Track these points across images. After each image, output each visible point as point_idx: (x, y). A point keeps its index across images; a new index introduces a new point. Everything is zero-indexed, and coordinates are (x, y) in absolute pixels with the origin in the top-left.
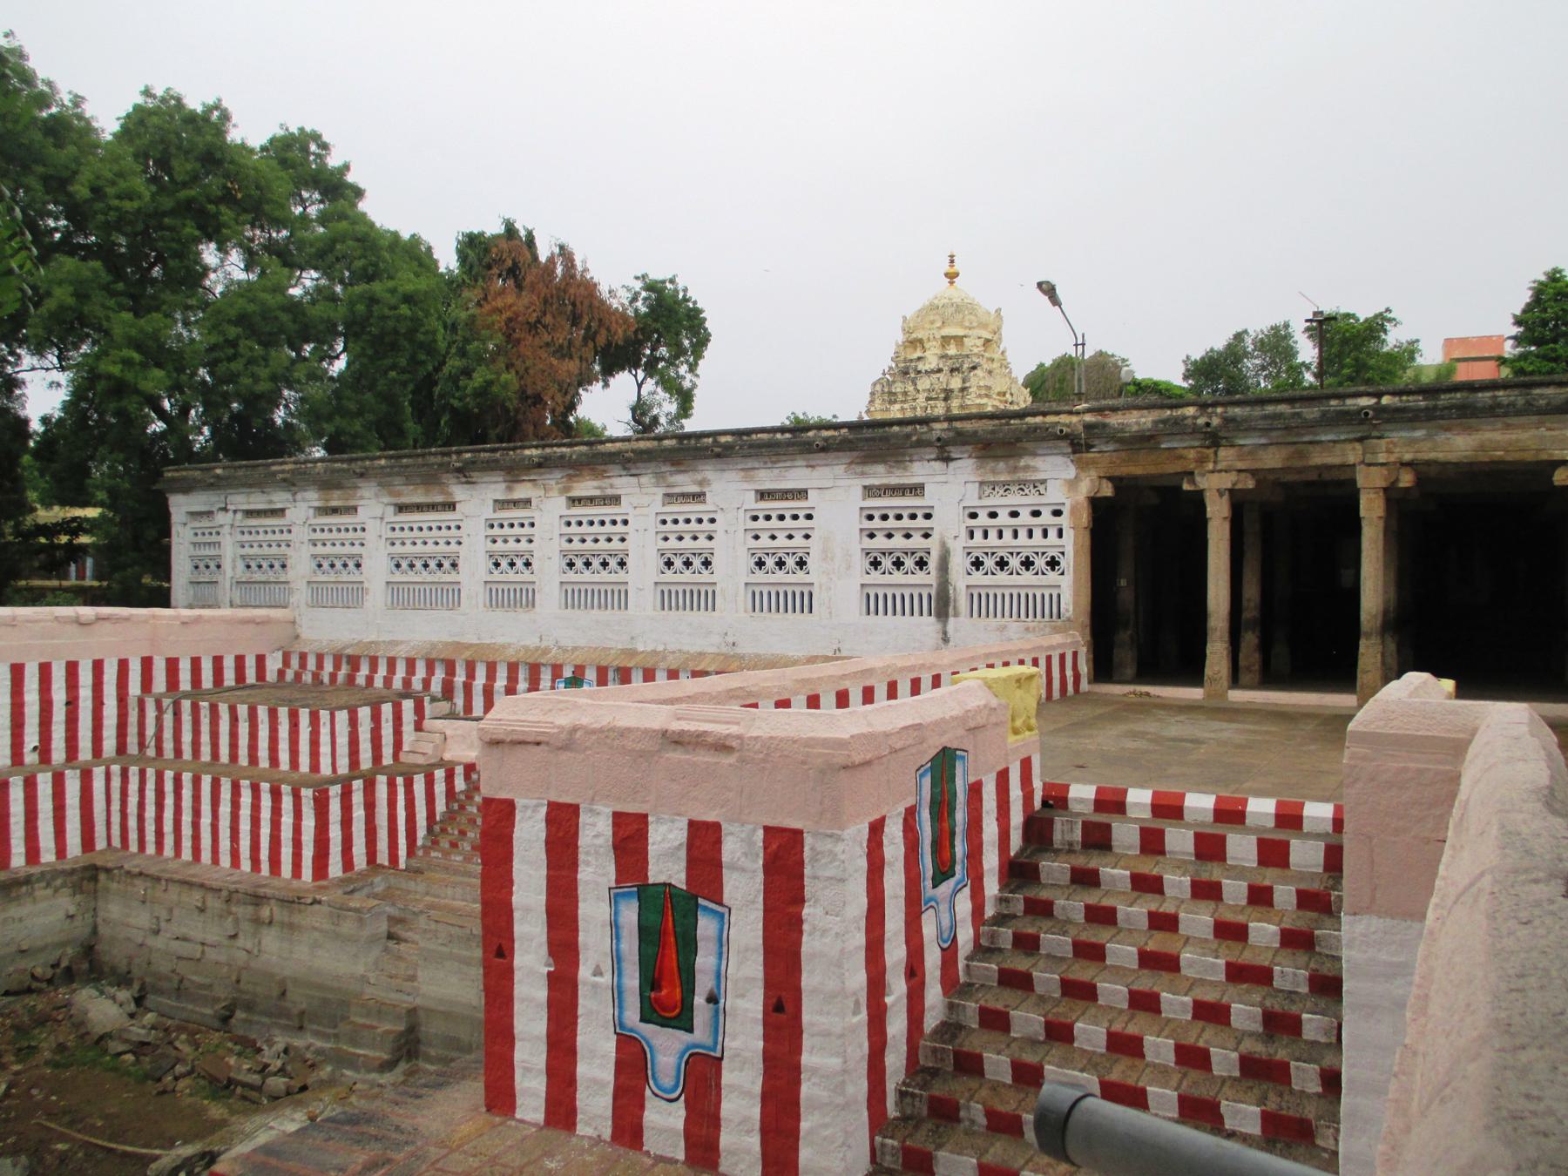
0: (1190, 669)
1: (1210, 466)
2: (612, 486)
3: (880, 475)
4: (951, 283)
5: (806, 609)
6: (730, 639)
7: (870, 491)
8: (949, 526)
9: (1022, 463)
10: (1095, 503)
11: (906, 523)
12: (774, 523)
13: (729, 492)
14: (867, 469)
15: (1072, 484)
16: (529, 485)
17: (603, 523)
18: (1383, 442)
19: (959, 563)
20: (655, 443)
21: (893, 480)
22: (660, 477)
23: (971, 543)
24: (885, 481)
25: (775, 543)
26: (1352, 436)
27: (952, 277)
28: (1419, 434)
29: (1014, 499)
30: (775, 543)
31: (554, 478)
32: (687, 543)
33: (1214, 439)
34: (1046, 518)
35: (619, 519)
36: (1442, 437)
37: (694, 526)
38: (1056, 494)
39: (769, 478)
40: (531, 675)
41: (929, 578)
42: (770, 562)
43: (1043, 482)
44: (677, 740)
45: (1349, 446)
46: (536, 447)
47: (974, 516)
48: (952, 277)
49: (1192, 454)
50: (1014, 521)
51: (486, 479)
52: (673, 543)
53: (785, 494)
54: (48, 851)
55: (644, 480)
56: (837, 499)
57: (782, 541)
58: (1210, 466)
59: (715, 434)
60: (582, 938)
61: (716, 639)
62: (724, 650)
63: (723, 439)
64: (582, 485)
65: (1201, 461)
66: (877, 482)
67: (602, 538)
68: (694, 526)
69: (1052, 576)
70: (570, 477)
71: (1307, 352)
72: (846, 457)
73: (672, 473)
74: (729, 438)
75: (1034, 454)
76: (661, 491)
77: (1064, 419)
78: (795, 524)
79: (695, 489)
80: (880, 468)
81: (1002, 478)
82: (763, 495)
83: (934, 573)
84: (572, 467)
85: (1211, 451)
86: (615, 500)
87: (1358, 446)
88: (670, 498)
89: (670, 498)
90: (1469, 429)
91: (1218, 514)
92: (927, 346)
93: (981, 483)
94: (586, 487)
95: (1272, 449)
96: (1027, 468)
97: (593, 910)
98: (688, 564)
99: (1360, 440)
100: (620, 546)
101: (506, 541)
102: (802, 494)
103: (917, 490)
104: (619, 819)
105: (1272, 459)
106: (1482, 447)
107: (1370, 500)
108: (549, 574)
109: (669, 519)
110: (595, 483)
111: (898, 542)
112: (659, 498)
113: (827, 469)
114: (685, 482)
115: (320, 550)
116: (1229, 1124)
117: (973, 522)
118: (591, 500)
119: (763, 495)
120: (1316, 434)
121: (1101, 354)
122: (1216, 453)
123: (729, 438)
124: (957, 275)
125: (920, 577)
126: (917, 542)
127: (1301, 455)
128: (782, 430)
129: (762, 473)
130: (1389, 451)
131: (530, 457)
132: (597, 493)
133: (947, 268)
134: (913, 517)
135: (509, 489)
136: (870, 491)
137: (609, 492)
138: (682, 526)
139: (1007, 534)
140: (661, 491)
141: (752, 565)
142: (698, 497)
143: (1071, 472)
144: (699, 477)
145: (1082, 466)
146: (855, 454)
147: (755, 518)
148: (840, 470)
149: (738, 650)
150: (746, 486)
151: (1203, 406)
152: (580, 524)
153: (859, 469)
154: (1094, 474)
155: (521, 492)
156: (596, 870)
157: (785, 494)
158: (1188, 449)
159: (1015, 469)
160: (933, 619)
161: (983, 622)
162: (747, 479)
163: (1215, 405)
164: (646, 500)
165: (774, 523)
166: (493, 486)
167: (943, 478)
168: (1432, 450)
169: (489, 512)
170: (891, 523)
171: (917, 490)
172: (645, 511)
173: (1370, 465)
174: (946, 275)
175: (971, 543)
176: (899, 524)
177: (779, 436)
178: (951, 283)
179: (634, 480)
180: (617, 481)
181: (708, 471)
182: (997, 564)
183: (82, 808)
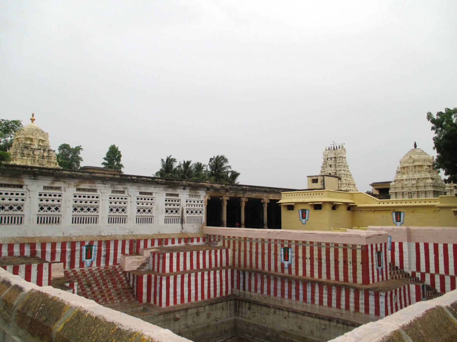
2: (95, 186)
3: (170, 191)
4: (32, 122)
5: (51, 222)
6: (132, 231)
7: (167, 195)
8: (183, 203)
9: (197, 191)
10: (208, 200)
11: (174, 202)
12: (143, 200)
13: (133, 192)
14: (168, 189)
15: (205, 197)
16: (62, 183)
17: (145, 199)
19: (185, 211)
20: (113, 176)
21: (173, 193)
22: (112, 186)
24: (171, 193)
25: (143, 206)
27: (33, 120)
29: (194, 199)
30: (87, 204)
31: (73, 182)
32: (118, 204)
33: (227, 191)
34: (200, 203)
36: (252, 194)
37: (120, 200)
38: (202, 198)
39: (144, 189)
40: (72, 245)
41: (180, 215)
42: (142, 210)
44: (379, 235)
46: (68, 171)
48: (33, 120)
49: (223, 193)
51: (44, 179)
52: (113, 204)
55: (107, 186)
56: (160, 196)
57: (89, 203)
61: (127, 231)
62: (130, 234)
63: (134, 178)
64: (84, 185)
65: (224, 194)
66: (169, 192)
67: (89, 202)
68: (120, 200)
69: (201, 215)
70: (80, 182)
72: (164, 186)
73: (117, 185)
74: (135, 178)
76: (111, 189)
77: (206, 184)
78: (145, 201)
79: (123, 190)
80: (171, 190)
81: (194, 194)
82: (141, 193)
83: (180, 214)
84: (83, 179)
88: (167, 195)
89: (113, 192)
90: (255, 193)
91: (243, 204)
92: (34, 141)
94: (86, 186)
96: (198, 193)
97: (374, 256)
98: (192, 212)
100: (124, 205)
101: (115, 203)
102: (151, 194)
103: (177, 195)
105: (233, 195)
106: (256, 196)
108: (67, 213)
110: (89, 185)
112: (111, 191)
113: (158, 189)
114: (120, 188)
115: (168, 206)
119: (141, 193)
123: (135, 178)
124: (34, 120)
125: (176, 215)
126: (176, 207)
127: (236, 195)
128: (150, 178)
129: (143, 188)
131: (66, 174)
132: (89, 188)
133: (31, 117)
134: (118, 198)
135: (52, 183)
137: (94, 188)
138: (116, 200)
139: (193, 206)
140: (111, 189)
141: (97, 209)
142: (123, 192)
143: (205, 194)
144: (125, 187)
145: (207, 193)
146: (166, 186)
147: (138, 199)
148: (162, 189)
149: (134, 234)
150: (137, 190)
151: (226, 185)
153: (166, 189)
154: (208, 195)
155: (57, 184)
156: (374, 251)
158: (222, 191)
159: (196, 193)
160: (180, 224)
161: (190, 224)
162: (138, 189)
164: (106, 191)
165: (143, 200)
166: (45, 181)
169: (41, 190)
170: (171, 202)
171: (177, 195)
172: (106, 195)
174: (31, 119)
176: (45, 197)
178: (32, 122)
179: (104, 185)
180: (97, 185)
181: (128, 186)
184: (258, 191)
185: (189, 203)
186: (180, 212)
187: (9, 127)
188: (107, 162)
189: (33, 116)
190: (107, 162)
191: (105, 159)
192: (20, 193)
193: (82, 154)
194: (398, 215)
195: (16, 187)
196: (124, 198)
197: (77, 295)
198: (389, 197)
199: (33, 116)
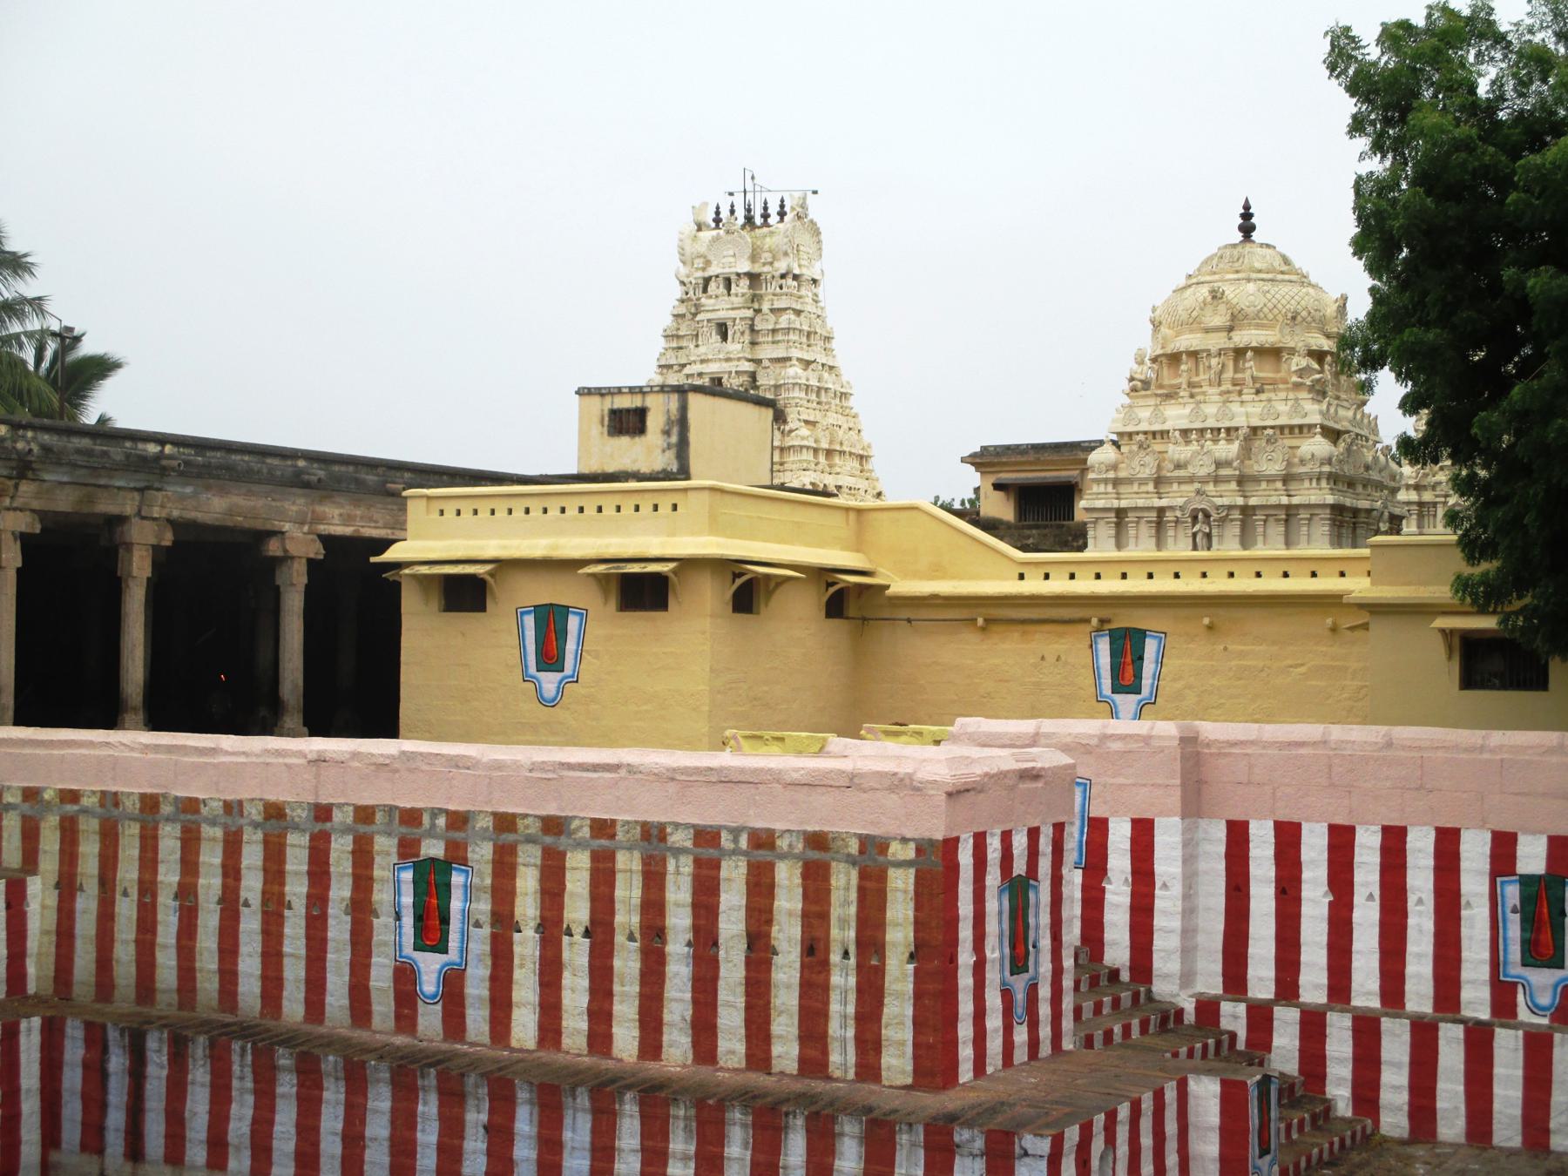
1: (7, 502)
18: (160, 495)
26: (132, 485)
28: (189, 490)
45: (130, 495)
54: (899, 995)
58: (7, 502)
59: (161, 439)
71: (1487, 566)
85: (11, 483)
87: (136, 495)
90: (223, 492)
91: (139, 568)
95: (68, 489)
99: (141, 490)
104: (1334, 830)
105: (64, 502)
106: (230, 512)
107: (141, 557)
116: (1461, 1027)
120: (111, 477)
122: (16, 487)
127: (91, 500)
130: (163, 506)
163: (26, 427)
168: (196, 509)
173: (144, 518)
177: (168, 449)
183: (1229, 856)
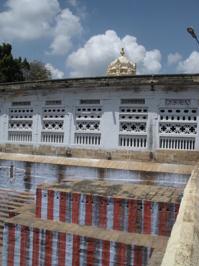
0: (129, 150)
23: (162, 121)
34: (190, 113)
35: (30, 110)
43: (189, 100)
47: (163, 111)
50: (178, 114)
53: (91, 102)
60: (179, 211)
75: (57, 91)
82: (82, 102)
86: (28, 103)
88: (123, 101)
93: (166, 99)
102: (98, 101)
109: (47, 110)
111: (89, 119)
112: (44, 103)
117: (162, 114)
118: (20, 103)
121: (8, 44)
126: (141, 120)
136: (123, 101)
152: (16, 111)
157: (91, 102)
167: (152, 97)
175: (162, 121)
182: (94, 126)
184: (174, 76)
185: (166, 113)
186: (147, 127)
187: (7, 49)
188: (22, 61)
189: (123, 50)
190: (22, 61)
191: (25, 60)
192: (97, 109)
193: (17, 58)
194: (152, 86)
195: (178, 102)
196: (61, 109)
197: (112, 231)
198: (122, 155)
199: (123, 50)
